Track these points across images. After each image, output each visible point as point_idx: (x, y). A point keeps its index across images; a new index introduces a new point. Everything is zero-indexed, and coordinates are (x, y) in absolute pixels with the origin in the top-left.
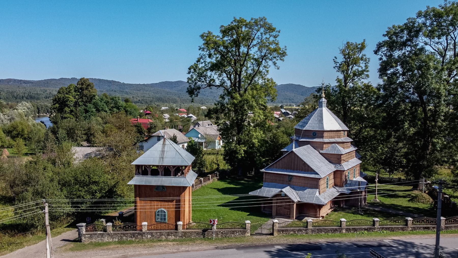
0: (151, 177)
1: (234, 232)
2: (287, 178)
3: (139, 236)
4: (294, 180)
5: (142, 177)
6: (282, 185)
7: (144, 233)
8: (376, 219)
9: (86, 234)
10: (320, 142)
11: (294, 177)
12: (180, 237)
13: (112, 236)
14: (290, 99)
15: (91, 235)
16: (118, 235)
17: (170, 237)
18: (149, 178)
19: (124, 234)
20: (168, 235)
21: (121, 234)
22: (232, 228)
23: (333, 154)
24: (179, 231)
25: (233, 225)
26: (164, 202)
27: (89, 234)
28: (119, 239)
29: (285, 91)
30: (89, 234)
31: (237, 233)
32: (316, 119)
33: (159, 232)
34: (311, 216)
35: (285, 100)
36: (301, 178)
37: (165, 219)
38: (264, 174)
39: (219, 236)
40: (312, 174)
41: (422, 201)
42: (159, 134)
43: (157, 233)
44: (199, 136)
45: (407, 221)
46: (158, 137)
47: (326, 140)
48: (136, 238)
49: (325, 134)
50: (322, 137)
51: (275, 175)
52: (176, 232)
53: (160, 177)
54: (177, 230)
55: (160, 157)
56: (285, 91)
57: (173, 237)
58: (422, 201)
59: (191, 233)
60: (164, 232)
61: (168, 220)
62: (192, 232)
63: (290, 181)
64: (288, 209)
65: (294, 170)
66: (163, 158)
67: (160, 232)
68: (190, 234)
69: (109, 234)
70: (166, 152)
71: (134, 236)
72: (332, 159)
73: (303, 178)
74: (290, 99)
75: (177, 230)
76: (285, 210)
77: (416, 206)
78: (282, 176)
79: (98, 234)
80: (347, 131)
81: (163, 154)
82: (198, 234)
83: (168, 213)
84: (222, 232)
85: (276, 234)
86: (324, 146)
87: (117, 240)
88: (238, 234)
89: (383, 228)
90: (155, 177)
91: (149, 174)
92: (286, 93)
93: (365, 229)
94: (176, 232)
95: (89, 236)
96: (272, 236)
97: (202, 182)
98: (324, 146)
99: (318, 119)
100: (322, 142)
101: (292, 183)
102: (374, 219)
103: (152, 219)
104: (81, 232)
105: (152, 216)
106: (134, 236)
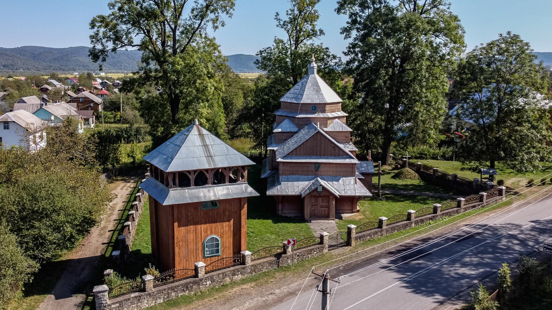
0: (196, 188)
1: (311, 250)
2: (313, 168)
3: (194, 286)
4: (322, 169)
5: (182, 190)
6: (307, 176)
7: (201, 280)
8: (438, 205)
9: (113, 304)
10: (324, 118)
11: (323, 165)
12: (248, 273)
13: (155, 295)
14: (84, 66)
15: (120, 302)
16: (164, 292)
17: (236, 276)
18: (193, 191)
19: (172, 289)
20: (234, 275)
21: (169, 289)
22: (307, 247)
23: (340, 132)
24: (248, 265)
25: (309, 241)
26: (424, 238)
27: (117, 303)
28: (164, 299)
29: (76, 55)
30: (117, 303)
31: (314, 251)
32: (312, 89)
33: (221, 273)
34: (347, 211)
35: (77, 67)
36: (332, 165)
37: (217, 251)
38: (281, 165)
39: (296, 260)
40: (345, 158)
41: (409, 176)
42: (7, 119)
43: (219, 274)
44: (53, 118)
45: (459, 202)
46: (5, 123)
47: (330, 115)
48: (190, 291)
49: (327, 108)
50: (324, 111)
51: (293, 165)
52: (244, 268)
53: (209, 187)
54: (245, 264)
55: (206, 156)
56: (76, 55)
57: (240, 276)
58: (409, 176)
59: (262, 265)
60: (228, 271)
61: (223, 252)
62: (264, 262)
63: (316, 170)
64: (325, 207)
65: (321, 156)
66: (211, 157)
67: (223, 273)
68: (261, 267)
69: (149, 294)
70: (210, 147)
71: (187, 288)
72: (339, 138)
73: (334, 165)
74: (84, 66)
75: (245, 264)
76: (322, 209)
77: (404, 183)
78: (307, 165)
79: (133, 298)
80: (341, 102)
81: (208, 152)
82: (270, 263)
83: (221, 240)
84: (298, 254)
85: (353, 243)
86: (329, 122)
87: (162, 301)
88: (315, 253)
89: (444, 214)
90: (203, 188)
91: (192, 185)
92: (77, 58)
93: (431, 219)
94: (244, 267)
95: (118, 305)
96: (348, 248)
97: (504, 193)
98: (329, 122)
99: (314, 89)
100: (326, 118)
101: (319, 173)
102: (435, 205)
103: (199, 255)
104: (104, 302)
105: (198, 250)
106: (187, 288)
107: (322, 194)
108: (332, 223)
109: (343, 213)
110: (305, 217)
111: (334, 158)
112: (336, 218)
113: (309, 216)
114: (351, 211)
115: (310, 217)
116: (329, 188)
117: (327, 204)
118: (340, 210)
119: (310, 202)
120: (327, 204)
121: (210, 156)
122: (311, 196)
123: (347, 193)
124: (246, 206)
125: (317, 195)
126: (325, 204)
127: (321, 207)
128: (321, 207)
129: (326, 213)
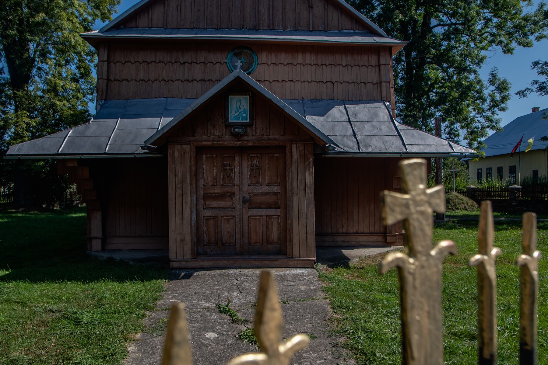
64: (269, 206)
76: (254, 212)
107: (250, 139)
108: (299, 278)
109: (351, 247)
110: (172, 256)
111: (298, 348)
112: (320, 259)
113: (188, 248)
114: (380, 239)
115: (196, 254)
116: (376, 29)
117: (276, 189)
118: (337, 234)
119: (196, 175)
120: (276, 189)
121: (345, 108)
122: (200, 150)
123: (367, 146)
124: (165, 121)
125: (228, 140)
126: (265, 189)
127: (250, 203)
128: (250, 203)
129: (275, 235)
